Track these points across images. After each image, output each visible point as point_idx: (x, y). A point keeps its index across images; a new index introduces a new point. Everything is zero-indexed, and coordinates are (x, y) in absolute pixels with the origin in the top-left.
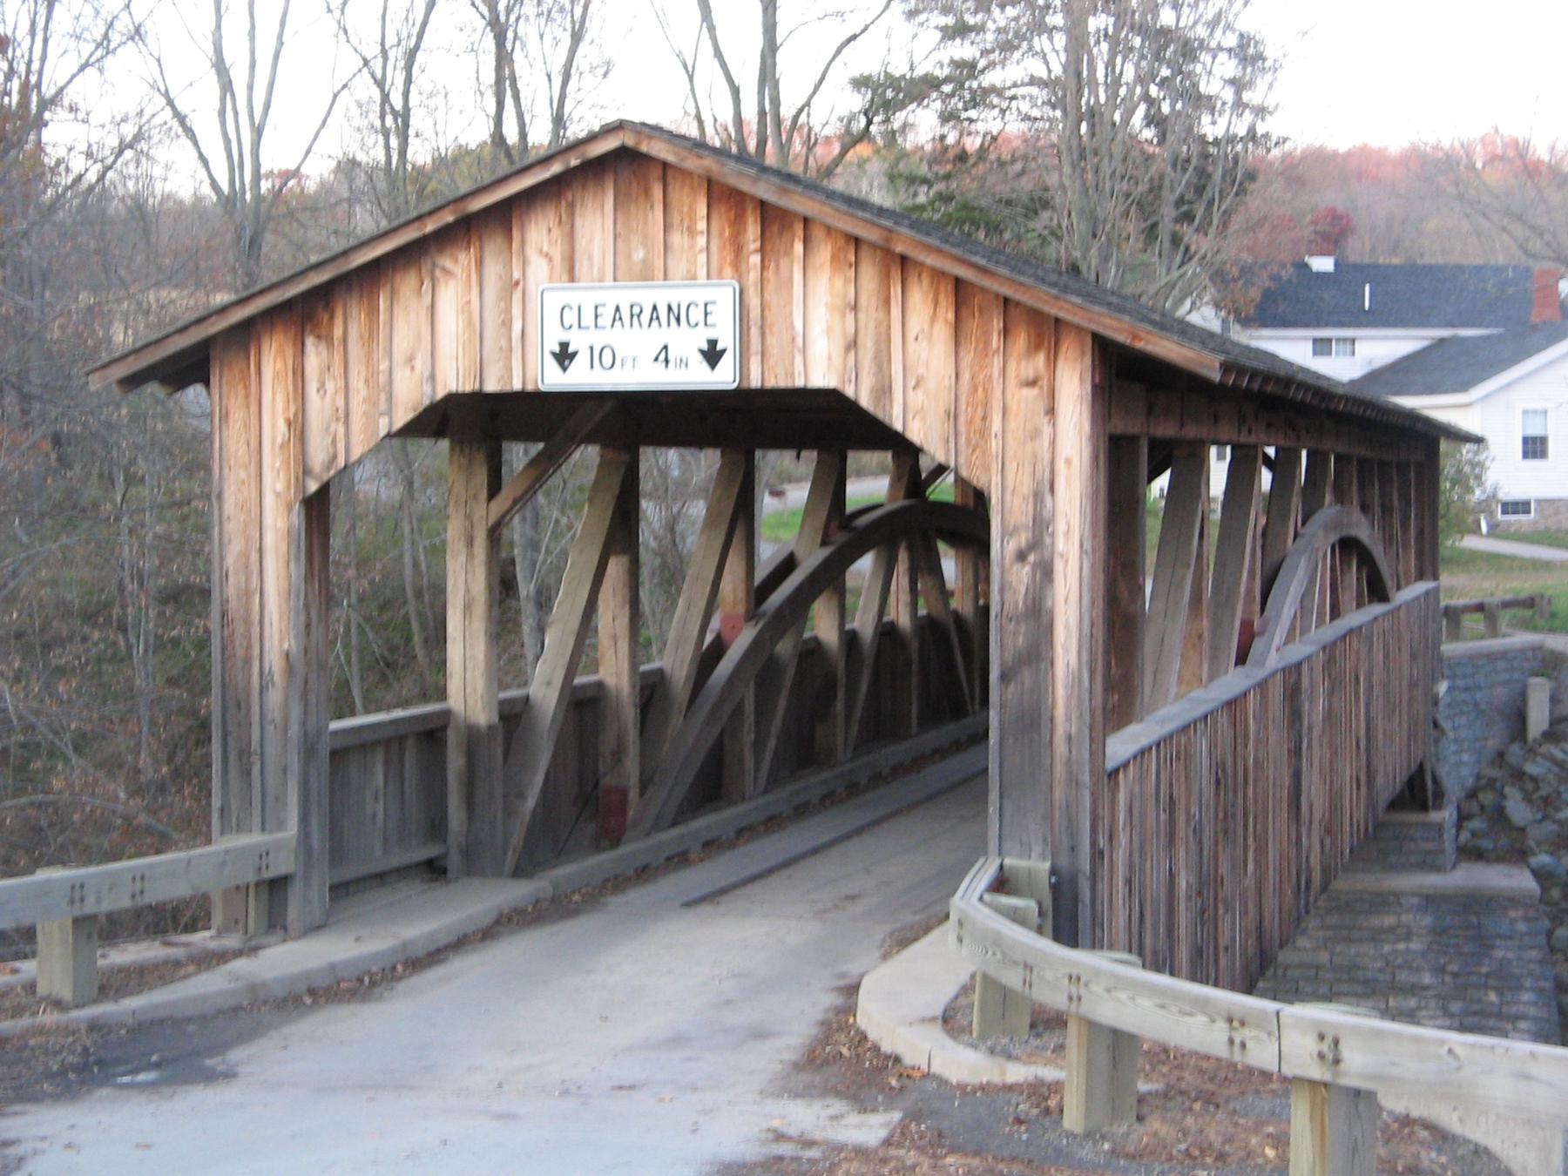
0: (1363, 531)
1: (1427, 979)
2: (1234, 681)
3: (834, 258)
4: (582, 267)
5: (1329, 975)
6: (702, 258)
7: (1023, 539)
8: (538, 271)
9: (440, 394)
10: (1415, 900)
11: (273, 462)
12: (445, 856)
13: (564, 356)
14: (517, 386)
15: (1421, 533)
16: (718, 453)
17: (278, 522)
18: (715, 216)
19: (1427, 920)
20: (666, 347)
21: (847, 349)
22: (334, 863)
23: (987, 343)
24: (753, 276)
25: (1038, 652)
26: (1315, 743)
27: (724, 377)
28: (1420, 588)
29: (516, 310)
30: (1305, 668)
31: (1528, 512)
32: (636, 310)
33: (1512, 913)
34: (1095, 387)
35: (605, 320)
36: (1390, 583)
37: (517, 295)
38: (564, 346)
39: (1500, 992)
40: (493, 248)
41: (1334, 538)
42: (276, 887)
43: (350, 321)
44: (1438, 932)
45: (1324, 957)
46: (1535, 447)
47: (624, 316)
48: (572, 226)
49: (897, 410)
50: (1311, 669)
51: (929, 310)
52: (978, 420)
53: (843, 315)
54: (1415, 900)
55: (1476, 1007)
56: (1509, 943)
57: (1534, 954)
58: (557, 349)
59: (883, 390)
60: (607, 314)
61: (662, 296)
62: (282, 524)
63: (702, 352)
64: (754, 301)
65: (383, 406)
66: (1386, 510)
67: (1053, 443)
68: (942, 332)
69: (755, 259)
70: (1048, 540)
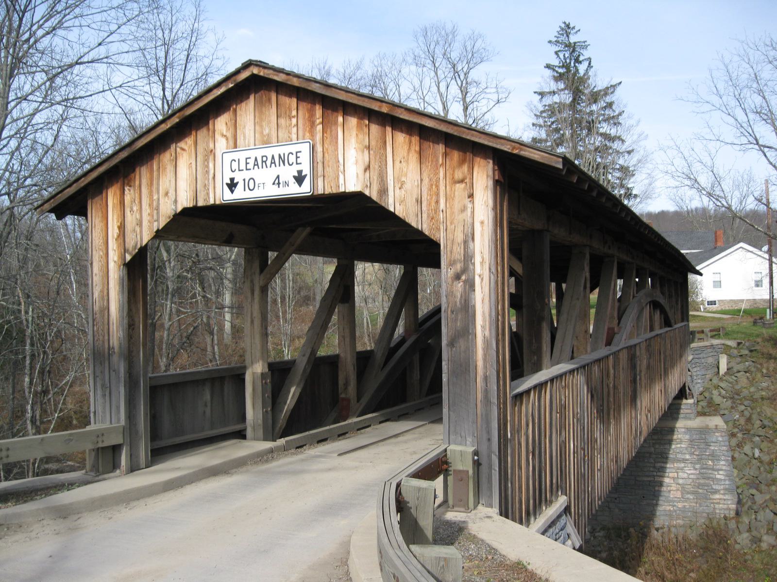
0: (662, 301)
1: (688, 457)
2: (603, 352)
3: (359, 127)
5: (654, 456)
6: (294, 130)
7: (459, 267)
8: (221, 144)
9: (179, 209)
10: (683, 430)
11: (113, 245)
12: (245, 430)
13: (232, 185)
14: (212, 202)
15: (682, 306)
16: (402, 267)
17: (115, 273)
18: (300, 108)
19: (687, 437)
20: (278, 177)
21: (365, 170)
23: (437, 161)
24: (319, 136)
25: (466, 331)
26: (643, 378)
27: (305, 189)
28: (683, 324)
29: (211, 165)
30: (638, 347)
31: (715, 304)
32: (264, 159)
33: (717, 434)
34: (497, 183)
35: (250, 166)
36: (672, 321)
37: (211, 158)
38: (232, 180)
39: (712, 460)
40: (202, 134)
41: (649, 299)
42: (116, 449)
43: (143, 174)
45: (652, 449)
46: (718, 284)
47: (259, 162)
48: (236, 121)
49: (391, 201)
50: (640, 348)
51: (406, 147)
52: (433, 204)
53: (363, 152)
54: (683, 430)
55: (705, 466)
56: (716, 444)
57: (725, 448)
58: (229, 182)
59: (383, 191)
60: (251, 162)
61: (276, 151)
62: (116, 276)
63: (294, 177)
64: (319, 148)
65: (155, 217)
66: (670, 296)
67: (473, 212)
69: (320, 127)
70: (471, 267)
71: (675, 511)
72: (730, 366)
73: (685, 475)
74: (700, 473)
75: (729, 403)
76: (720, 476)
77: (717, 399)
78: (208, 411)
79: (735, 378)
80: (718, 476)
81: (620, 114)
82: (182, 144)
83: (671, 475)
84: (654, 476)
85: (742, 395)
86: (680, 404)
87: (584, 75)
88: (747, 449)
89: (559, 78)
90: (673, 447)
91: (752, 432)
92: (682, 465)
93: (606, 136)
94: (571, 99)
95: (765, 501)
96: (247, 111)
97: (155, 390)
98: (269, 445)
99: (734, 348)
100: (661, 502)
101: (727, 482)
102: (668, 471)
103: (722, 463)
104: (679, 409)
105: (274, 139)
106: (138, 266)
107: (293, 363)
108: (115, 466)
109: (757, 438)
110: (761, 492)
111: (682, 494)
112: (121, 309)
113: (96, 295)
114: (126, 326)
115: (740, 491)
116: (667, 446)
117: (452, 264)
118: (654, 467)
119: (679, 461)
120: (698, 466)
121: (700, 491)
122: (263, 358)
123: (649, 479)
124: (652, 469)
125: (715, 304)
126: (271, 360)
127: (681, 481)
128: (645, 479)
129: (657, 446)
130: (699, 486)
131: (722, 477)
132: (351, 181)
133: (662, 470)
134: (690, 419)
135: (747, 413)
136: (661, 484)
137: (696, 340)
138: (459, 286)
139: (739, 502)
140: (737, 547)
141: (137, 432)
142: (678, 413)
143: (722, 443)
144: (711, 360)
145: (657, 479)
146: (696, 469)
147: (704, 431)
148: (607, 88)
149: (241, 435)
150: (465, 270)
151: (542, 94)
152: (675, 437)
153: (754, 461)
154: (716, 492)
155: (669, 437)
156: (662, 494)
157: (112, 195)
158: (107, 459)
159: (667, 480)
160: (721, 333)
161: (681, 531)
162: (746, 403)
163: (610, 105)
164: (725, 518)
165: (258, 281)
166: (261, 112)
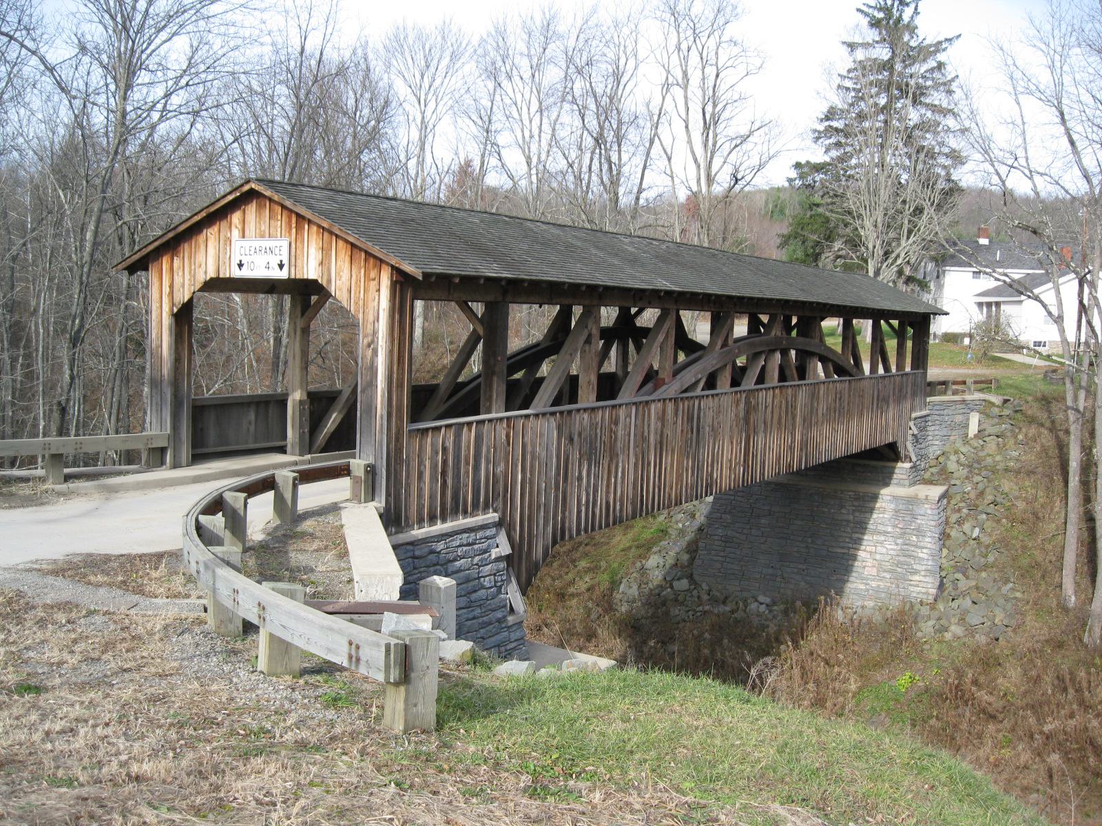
1: (890, 529)
4: (247, 233)
5: (852, 525)
8: (236, 233)
9: (208, 278)
10: (889, 498)
11: (165, 300)
12: (286, 446)
13: (240, 265)
14: (228, 276)
17: (167, 321)
19: (893, 506)
22: (194, 446)
27: (283, 275)
31: (1044, 346)
33: (926, 506)
35: (252, 252)
40: (224, 224)
42: (163, 450)
44: (897, 511)
45: (851, 517)
54: (889, 498)
59: (329, 281)
68: (347, 259)
69: (294, 230)
71: (868, 590)
72: (982, 427)
73: (884, 551)
74: (902, 550)
75: (964, 472)
76: (923, 554)
77: (952, 466)
78: (252, 428)
79: (982, 443)
80: (921, 555)
81: (953, 80)
82: (210, 230)
83: (868, 548)
84: (849, 548)
85: (983, 464)
86: (895, 468)
87: (909, 22)
88: (966, 527)
89: (875, 24)
90: (875, 516)
91: (980, 509)
92: (883, 538)
93: (934, 108)
94: (890, 54)
95: (970, 588)
96: (251, 209)
97: (200, 411)
98: (301, 458)
99: (998, 406)
100: (851, 579)
101: (930, 563)
102: (865, 543)
103: (928, 540)
104: (893, 473)
105: (267, 235)
106: (183, 315)
107: (340, 392)
108: (162, 463)
109: (984, 516)
110: (967, 578)
111: (878, 571)
112: (170, 348)
113: (154, 336)
114: (173, 361)
115: (943, 574)
116: (867, 515)
117: (365, 336)
118: (851, 538)
119: (879, 533)
120: (899, 541)
121: (899, 570)
122: (301, 388)
123: (843, 551)
124: (847, 540)
125: (1044, 346)
126: (312, 388)
127: (878, 557)
128: (839, 550)
129: (857, 514)
130: (898, 564)
131: (925, 556)
132: (311, 272)
133: (858, 542)
134: (904, 486)
135: (981, 486)
136: (854, 558)
137: (950, 392)
138: (369, 352)
139: (941, 586)
140: (919, 634)
141: (180, 439)
142: (890, 478)
143: (931, 517)
144: (959, 418)
145: (852, 551)
146: (897, 544)
147: (912, 501)
148: (940, 43)
149: (282, 450)
150: (373, 342)
151: (852, 46)
152: (878, 505)
153: (972, 542)
154: (916, 572)
155: (871, 505)
156: (855, 569)
157: (165, 261)
158: (157, 457)
159: (861, 554)
160: (993, 386)
161: (868, 612)
162: (984, 473)
163: (940, 66)
164: (921, 603)
165: (300, 323)
166: (260, 214)
